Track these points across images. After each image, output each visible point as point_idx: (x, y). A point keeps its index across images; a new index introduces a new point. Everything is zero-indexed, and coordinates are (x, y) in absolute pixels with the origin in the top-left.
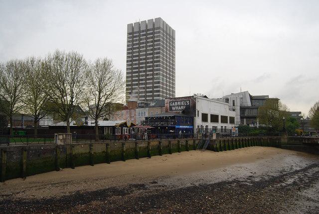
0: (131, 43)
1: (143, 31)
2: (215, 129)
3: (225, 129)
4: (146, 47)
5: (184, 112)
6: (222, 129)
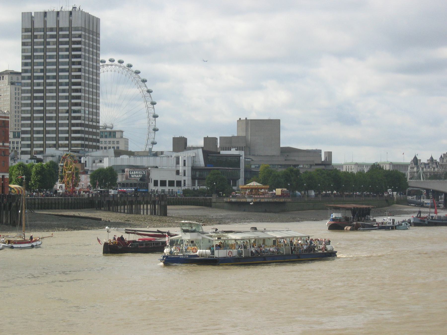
0: (29, 40)
1: (51, 30)
2: (163, 191)
3: (172, 192)
4: (58, 57)
5: (141, 179)
6: (169, 192)
